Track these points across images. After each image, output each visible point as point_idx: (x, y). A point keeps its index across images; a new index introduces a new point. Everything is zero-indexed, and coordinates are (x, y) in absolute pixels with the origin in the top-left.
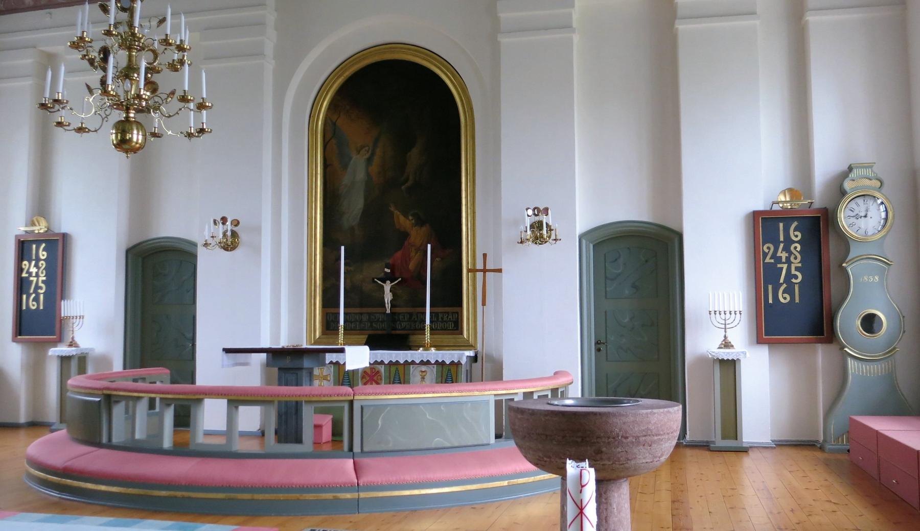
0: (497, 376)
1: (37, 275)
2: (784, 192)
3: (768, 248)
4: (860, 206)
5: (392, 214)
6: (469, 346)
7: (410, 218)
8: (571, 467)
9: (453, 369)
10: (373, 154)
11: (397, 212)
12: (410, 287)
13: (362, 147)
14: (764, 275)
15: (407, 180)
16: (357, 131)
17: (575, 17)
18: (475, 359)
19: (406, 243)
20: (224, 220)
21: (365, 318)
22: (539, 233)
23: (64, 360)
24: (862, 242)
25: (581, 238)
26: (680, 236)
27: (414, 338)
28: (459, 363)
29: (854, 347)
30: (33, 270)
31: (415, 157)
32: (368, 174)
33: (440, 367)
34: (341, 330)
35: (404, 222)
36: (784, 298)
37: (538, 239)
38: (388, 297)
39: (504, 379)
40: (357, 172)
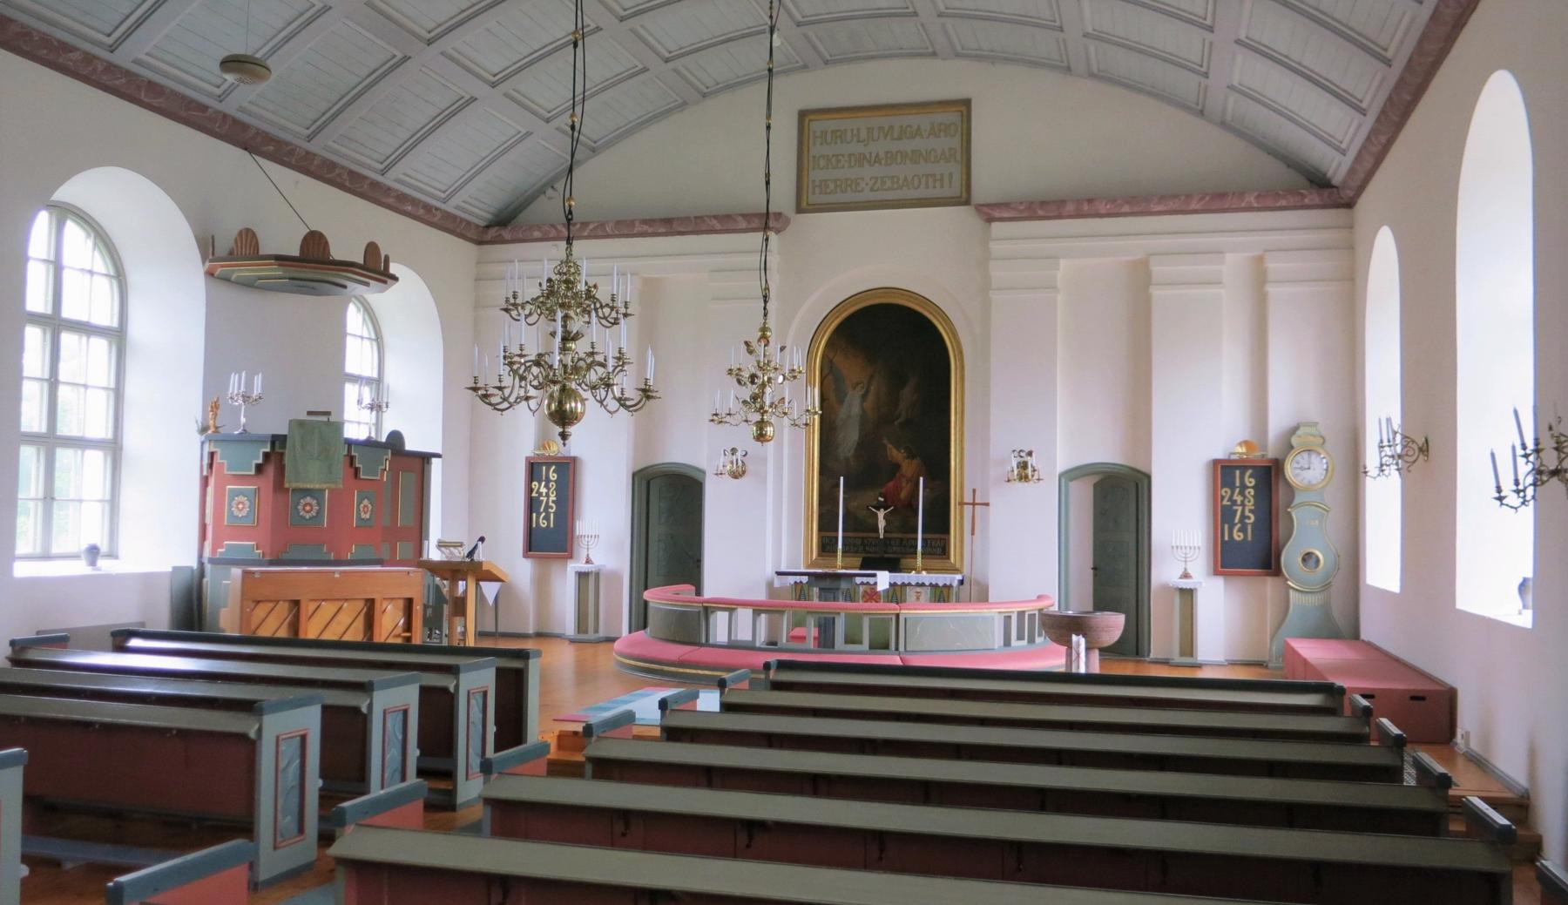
0: (983, 597)
1: (547, 495)
2: (1240, 444)
3: (1226, 492)
4: (1303, 459)
6: (956, 570)
8: (1074, 638)
12: (903, 514)
14: (1222, 516)
16: (853, 369)
17: (1059, 275)
18: (961, 582)
20: (734, 451)
22: (1024, 472)
23: (582, 576)
24: (1309, 488)
25: (1061, 476)
26: (1149, 477)
27: (905, 562)
29: (1297, 581)
30: (544, 490)
31: (907, 394)
32: (863, 409)
34: (840, 553)
35: (896, 454)
36: (1238, 536)
37: (1023, 478)
38: (882, 524)
39: (991, 600)
40: (853, 407)
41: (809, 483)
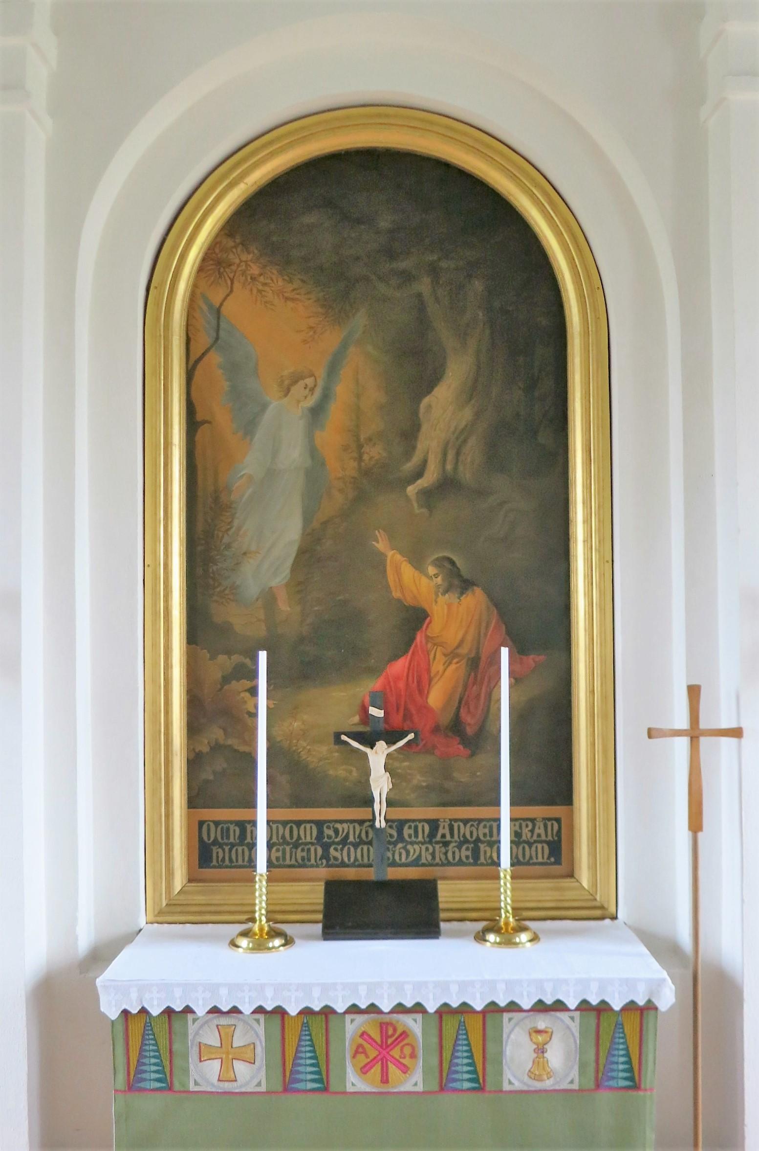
5: (379, 563)
7: (432, 570)
9: (630, 1025)
10: (326, 396)
11: (393, 556)
13: (296, 379)
15: (419, 474)
16: (277, 321)
19: (419, 637)
21: (309, 834)
28: (650, 1006)
31: (445, 408)
32: (313, 451)
33: (592, 1017)
35: (414, 581)
40: (282, 454)
41: (155, 614)
